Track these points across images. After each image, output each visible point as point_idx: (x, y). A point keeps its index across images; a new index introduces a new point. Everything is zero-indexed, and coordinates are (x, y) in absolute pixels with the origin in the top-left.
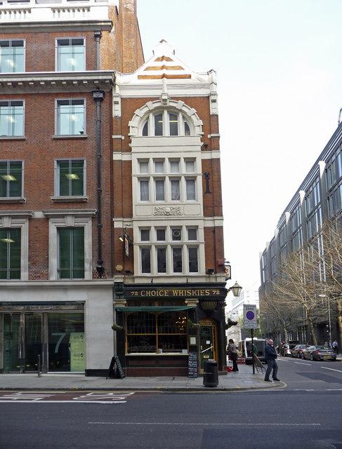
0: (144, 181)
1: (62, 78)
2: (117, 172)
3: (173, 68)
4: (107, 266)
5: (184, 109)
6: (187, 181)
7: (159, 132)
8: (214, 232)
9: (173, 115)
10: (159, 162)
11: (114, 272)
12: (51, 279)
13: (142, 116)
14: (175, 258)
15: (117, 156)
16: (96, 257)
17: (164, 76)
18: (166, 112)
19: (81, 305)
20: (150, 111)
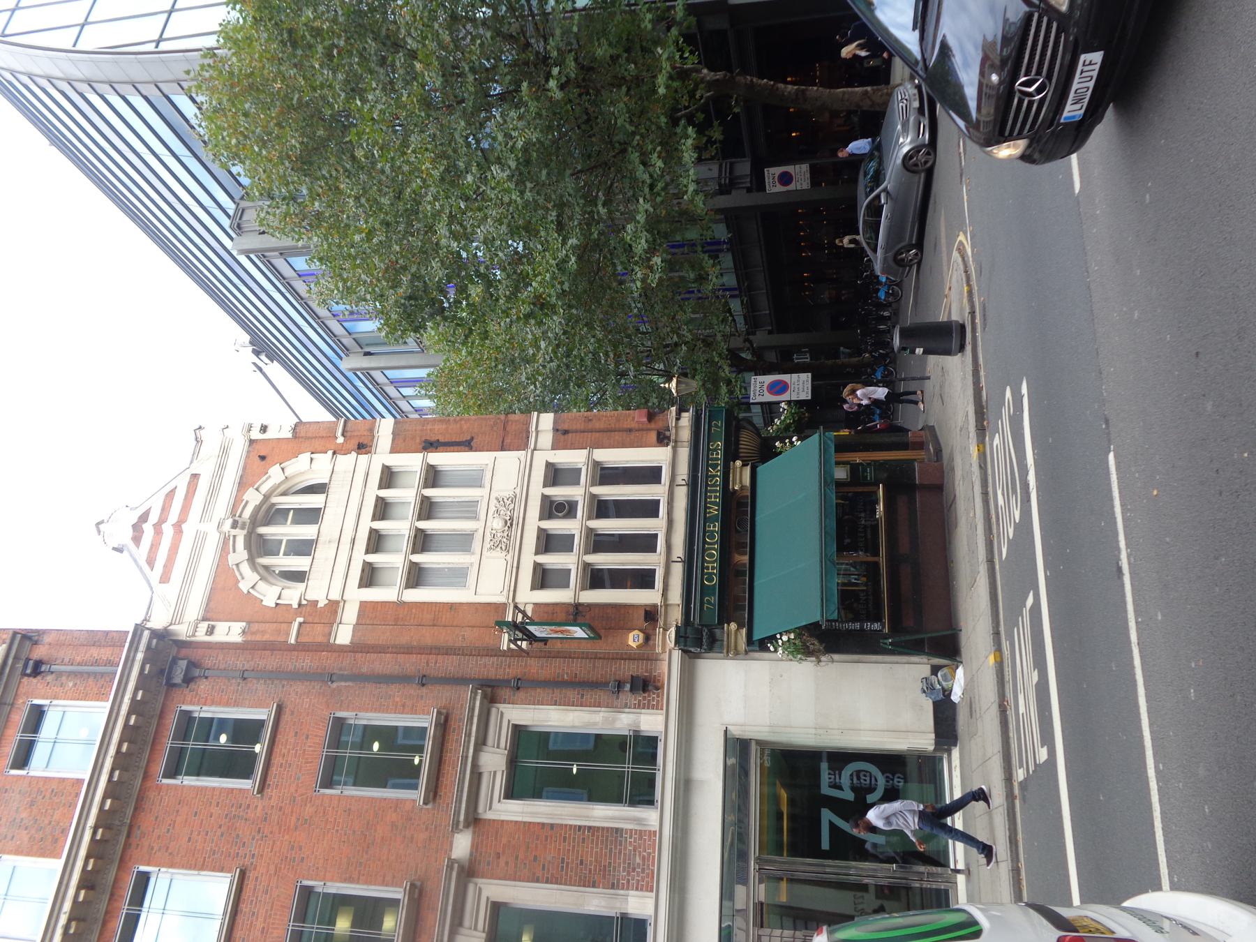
0: (416, 576)
1: (112, 751)
2: (383, 635)
3: (165, 509)
4: (629, 669)
5: (265, 488)
6: (434, 484)
7: (304, 548)
8: (566, 432)
9: (270, 514)
10: (376, 542)
11: (647, 654)
12: (661, 728)
13: (256, 577)
14: (619, 515)
15: (344, 636)
16: (601, 695)
17: (178, 527)
18: (262, 530)
19: (738, 748)
20: (251, 561)
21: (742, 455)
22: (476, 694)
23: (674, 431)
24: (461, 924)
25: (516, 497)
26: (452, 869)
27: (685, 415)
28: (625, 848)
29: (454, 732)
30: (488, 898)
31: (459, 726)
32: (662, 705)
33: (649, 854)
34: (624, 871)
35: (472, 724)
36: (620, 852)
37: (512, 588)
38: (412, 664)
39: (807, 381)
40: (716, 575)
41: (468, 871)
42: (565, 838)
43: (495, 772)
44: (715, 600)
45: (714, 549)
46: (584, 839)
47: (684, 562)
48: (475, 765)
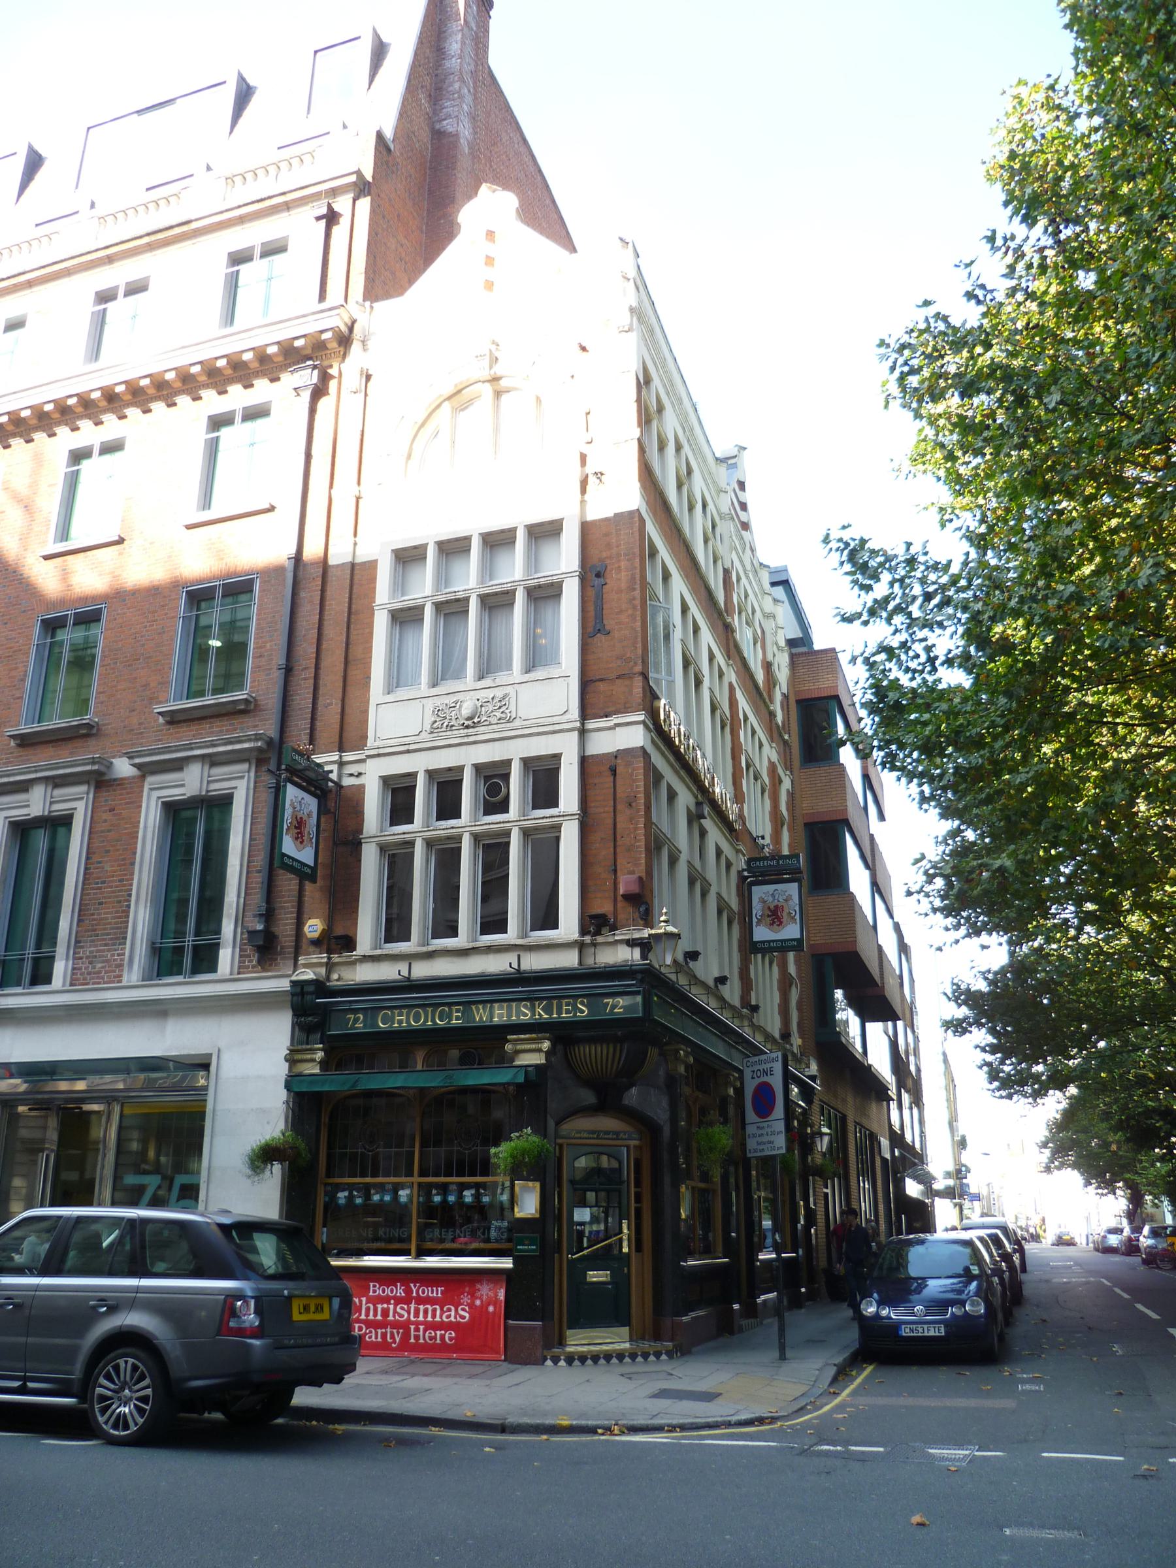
4: (284, 928)
8: (614, 771)
21: (582, 1048)
22: (256, 740)
23: (611, 939)
24: (56, 786)
25: (508, 722)
26: (93, 763)
27: (637, 953)
28: (109, 950)
29: (230, 725)
30: (75, 809)
31: (236, 730)
32: (244, 973)
33: (103, 978)
34: (90, 952)
35: (225, 744)
36: (106, 945)
37: (381, 751)
38: (306, 649)
39: (773, 1148)
40: (448, 1023)
41: (100, 781)
42: (122, 880)
43: (183, 786)
44: (357, 1028)
45: (426, 1020)
46: (120, 902)
47: (518, 971)
48: (188, 760)
